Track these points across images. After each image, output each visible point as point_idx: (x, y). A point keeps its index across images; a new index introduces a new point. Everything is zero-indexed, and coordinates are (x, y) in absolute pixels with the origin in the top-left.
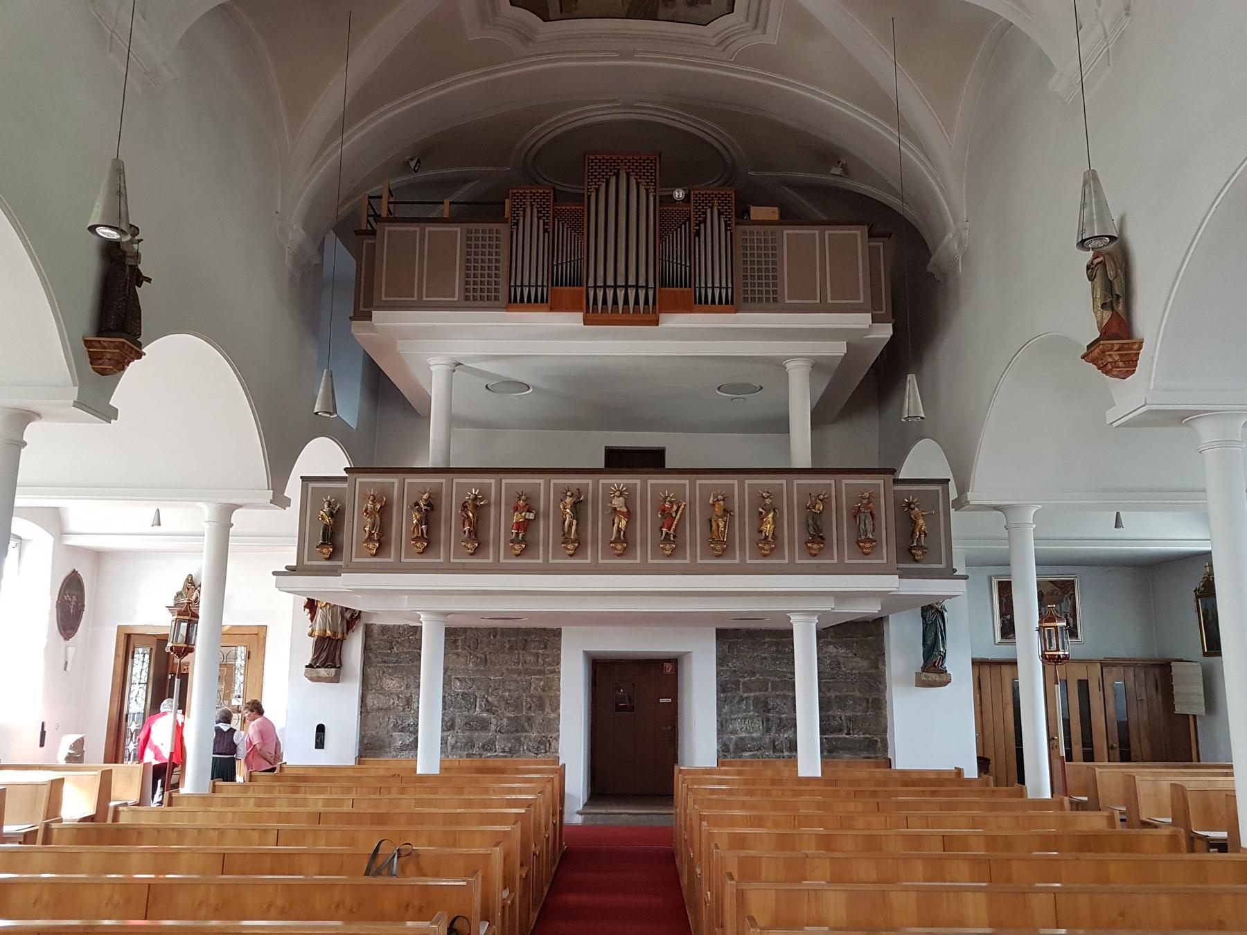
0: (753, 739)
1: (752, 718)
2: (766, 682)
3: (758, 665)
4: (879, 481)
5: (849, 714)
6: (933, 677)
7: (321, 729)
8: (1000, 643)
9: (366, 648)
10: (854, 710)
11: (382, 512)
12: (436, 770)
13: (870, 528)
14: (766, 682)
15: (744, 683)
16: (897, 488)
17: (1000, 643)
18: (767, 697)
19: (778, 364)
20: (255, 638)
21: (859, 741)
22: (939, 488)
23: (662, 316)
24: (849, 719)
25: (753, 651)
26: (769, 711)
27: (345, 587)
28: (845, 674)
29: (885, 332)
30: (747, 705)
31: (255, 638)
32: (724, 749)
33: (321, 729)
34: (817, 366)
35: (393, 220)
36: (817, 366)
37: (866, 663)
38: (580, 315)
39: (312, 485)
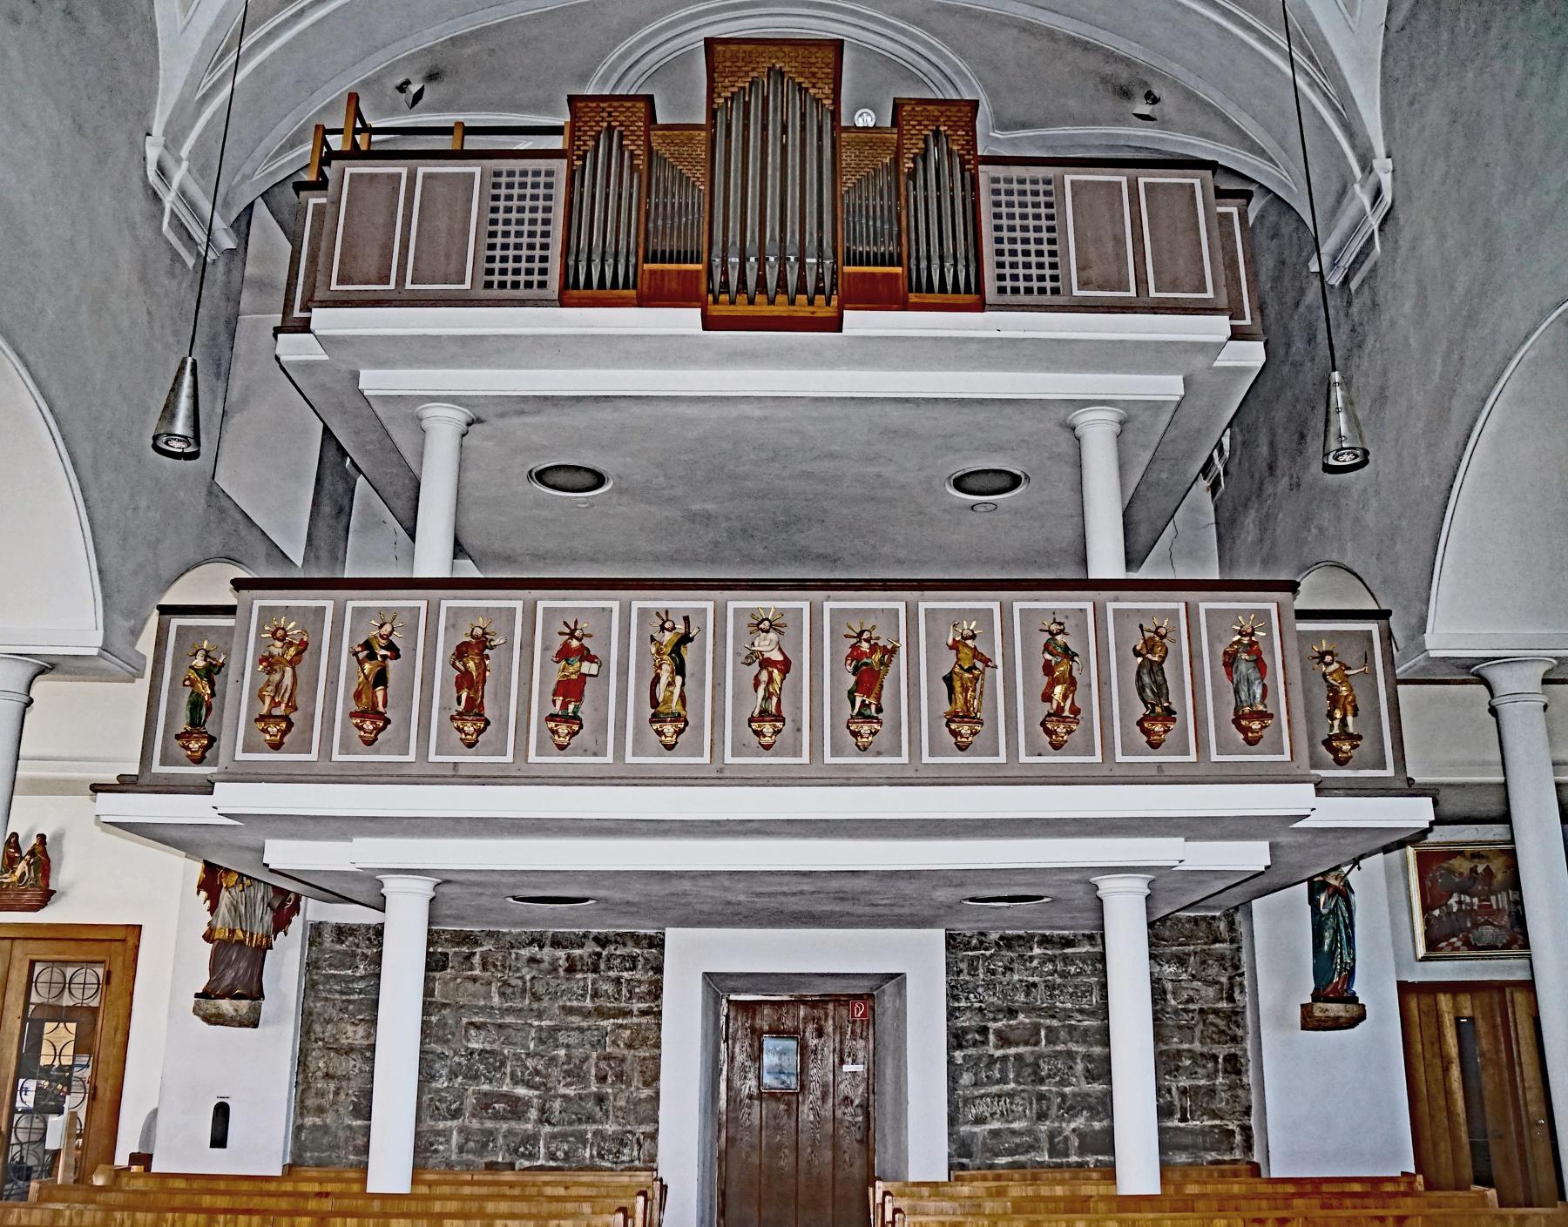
0: (1014, 1132)
1: (1011, 1095)
2: (1036, 1028)
3: (1021, 997)
4: (1269, 603)
5: (1184, 1082)
6: (1335, 1009)
7: (222, 1112)
8: (1425, 959)
9: (311, 965)
10: (1193, 1075)
11: (288, 655)
12: (402, 1185)
13: (1258, 692)
14: (1036, 1028)
15: (998, 1033)
16: (1303, 626)
17: (1425, 959)
18: (1040, 1056)
19: (1063, 420)
20: (117, 948)
21: (1203, 1132)
22: (1373, 627)
23: (849, 316)
24: (1184, 1092)
25: (1023, 958)
26: (1042, 1081)
27: (369, 917)
28: (1176, 1012)
29: (1253, 355)
30: (1003, 1071)
31: (117, 948)
32: (961, 1152)
33: (222, 1112)
34: (1129, 420)
35: (355, 154)
36: (1129, 420)
37: (1211, 992)
38: (695, 314)
39: (176, 622)
